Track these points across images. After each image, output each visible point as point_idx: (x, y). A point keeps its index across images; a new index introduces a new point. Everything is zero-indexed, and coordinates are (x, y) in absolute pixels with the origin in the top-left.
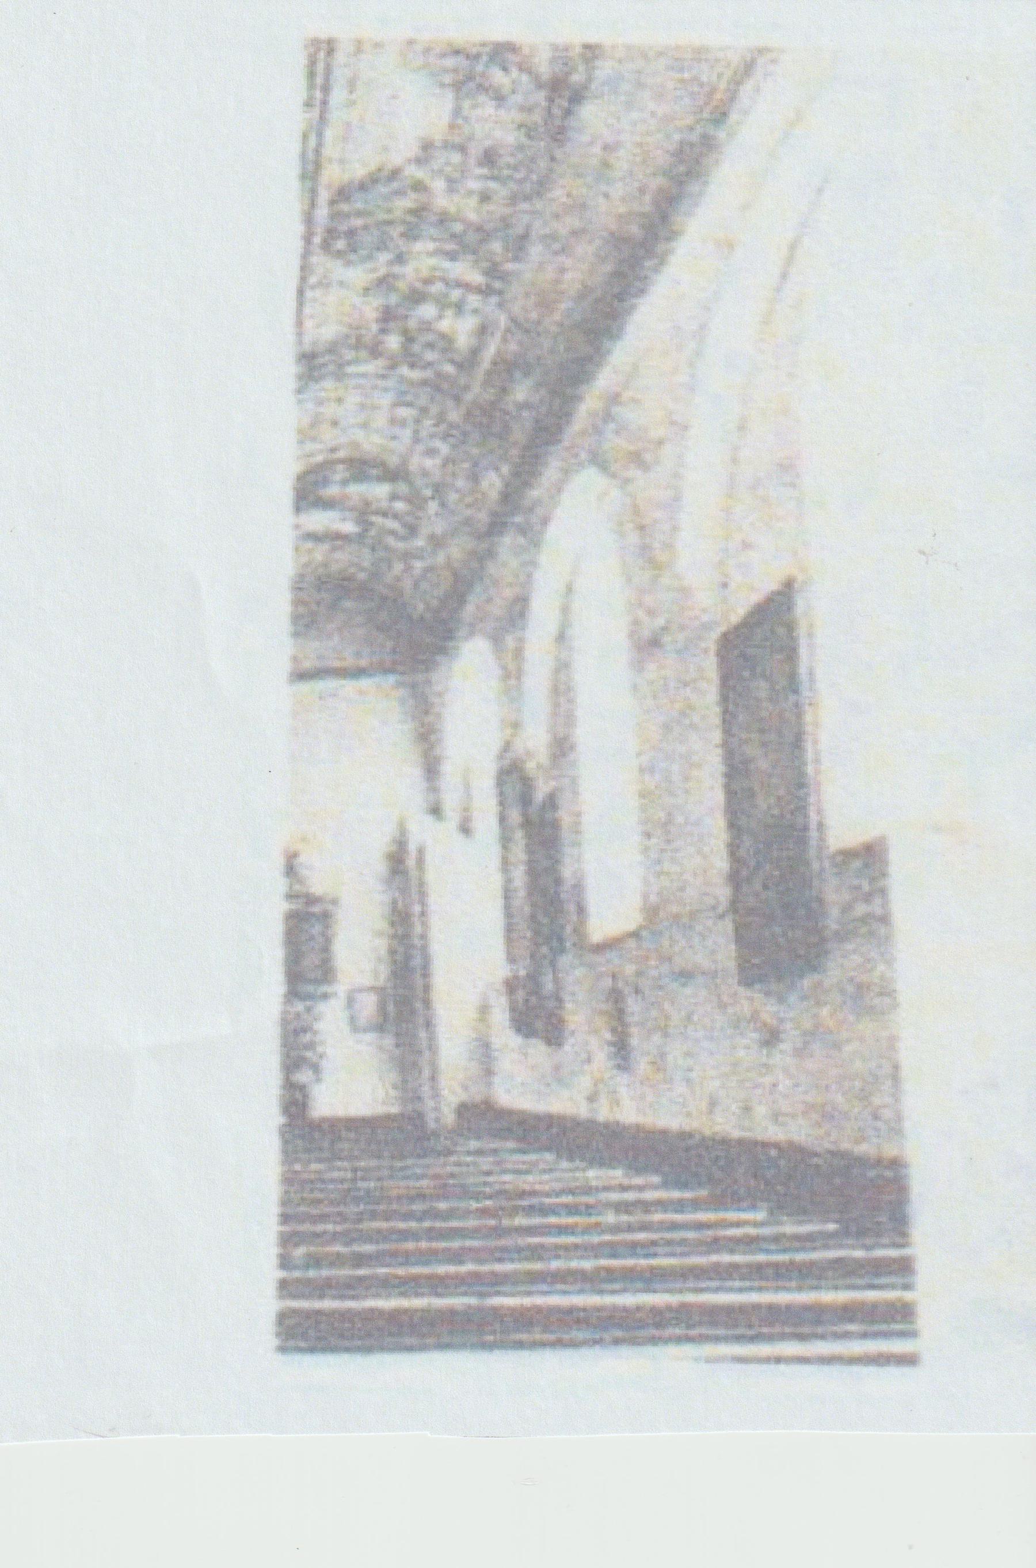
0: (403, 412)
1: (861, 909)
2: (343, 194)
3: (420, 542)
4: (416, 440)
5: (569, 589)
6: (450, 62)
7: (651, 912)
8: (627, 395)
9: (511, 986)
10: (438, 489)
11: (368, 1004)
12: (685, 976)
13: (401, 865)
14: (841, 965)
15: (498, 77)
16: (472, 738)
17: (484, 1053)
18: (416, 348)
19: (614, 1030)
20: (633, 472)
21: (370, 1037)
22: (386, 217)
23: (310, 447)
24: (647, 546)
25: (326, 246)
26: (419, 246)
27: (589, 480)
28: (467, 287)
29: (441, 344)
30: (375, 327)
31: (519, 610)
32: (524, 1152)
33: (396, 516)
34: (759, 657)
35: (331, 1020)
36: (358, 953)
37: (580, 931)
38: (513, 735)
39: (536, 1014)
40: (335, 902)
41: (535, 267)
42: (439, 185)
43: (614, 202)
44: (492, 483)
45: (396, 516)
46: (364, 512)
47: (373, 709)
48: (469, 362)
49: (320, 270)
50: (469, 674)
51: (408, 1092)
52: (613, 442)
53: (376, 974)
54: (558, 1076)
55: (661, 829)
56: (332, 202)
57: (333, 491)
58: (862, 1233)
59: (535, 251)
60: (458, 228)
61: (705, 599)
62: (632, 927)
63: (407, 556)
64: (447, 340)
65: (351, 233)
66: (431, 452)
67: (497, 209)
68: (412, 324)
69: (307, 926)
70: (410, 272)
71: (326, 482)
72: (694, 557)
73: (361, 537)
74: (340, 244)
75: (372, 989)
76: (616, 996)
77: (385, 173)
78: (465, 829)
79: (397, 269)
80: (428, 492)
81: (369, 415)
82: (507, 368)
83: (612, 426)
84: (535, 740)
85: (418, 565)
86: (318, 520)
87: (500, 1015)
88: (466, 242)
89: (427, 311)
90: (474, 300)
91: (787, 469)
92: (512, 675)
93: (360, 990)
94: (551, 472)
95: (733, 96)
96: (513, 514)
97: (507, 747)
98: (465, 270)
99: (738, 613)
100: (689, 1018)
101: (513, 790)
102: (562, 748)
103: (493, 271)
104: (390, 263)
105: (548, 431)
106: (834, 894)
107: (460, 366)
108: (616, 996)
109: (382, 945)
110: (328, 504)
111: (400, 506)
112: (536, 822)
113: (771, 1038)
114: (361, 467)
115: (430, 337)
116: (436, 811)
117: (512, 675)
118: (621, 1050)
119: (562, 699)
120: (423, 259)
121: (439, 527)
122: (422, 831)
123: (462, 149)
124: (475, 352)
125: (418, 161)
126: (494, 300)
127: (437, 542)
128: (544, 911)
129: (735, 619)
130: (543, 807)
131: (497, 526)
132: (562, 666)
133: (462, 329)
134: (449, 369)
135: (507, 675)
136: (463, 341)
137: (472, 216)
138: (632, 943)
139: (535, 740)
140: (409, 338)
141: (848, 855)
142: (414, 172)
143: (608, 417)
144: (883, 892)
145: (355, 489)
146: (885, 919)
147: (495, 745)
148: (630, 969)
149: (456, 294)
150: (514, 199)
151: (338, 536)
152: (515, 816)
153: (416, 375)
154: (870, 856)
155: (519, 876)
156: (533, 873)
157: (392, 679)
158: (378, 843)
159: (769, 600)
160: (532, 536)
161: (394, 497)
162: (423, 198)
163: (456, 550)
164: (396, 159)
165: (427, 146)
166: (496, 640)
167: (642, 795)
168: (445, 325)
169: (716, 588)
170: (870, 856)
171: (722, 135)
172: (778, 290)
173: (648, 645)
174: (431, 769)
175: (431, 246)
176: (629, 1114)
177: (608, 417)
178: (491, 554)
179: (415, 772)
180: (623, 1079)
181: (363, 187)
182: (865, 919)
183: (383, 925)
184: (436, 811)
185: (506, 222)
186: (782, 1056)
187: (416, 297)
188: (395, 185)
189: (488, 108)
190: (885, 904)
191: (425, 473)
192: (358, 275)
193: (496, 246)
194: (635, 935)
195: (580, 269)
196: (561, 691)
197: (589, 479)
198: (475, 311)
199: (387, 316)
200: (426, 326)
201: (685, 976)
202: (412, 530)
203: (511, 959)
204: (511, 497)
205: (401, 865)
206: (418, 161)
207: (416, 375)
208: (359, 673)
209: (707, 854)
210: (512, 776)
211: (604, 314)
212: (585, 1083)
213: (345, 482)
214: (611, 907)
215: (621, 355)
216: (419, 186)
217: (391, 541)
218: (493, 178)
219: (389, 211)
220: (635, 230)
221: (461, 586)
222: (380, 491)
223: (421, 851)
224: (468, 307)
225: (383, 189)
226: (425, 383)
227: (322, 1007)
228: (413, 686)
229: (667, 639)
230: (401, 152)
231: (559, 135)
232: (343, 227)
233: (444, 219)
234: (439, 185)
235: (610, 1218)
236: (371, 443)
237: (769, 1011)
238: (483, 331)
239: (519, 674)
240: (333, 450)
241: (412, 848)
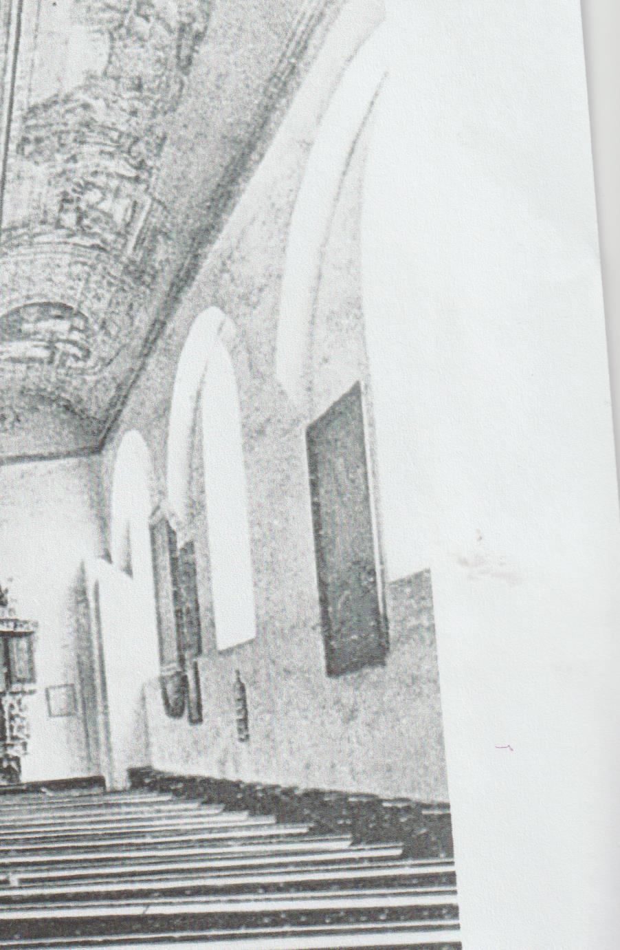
0: (77, 269)
1: (413, 622)
2: (33, 110)
3: (90, 363)
4: (87, 288)
5: (199, 395)
6: (107, 15)
7: (262, 627)
8: (236, 255)
11: (60, 699)
13: (82, 596)
14: (400, 658)
15: (141, 26)
16: (131, 504)
17: (143, 729)
18: (86, 222)
20: (244, 309)
22: (63, 128)
24: (253, 360)
25: (20, 149)
26: (86, 149)
28: (122, 177)
29: (103, 218)
30: (56, 209)
31: (164, 410)
32: (175, 803)
33: (74, 343)
34: (334, 438)
39: (182, 701)
40: (36, 625)
41: (166, 163)
42: (99, 105)
43: (227, 114)
44: (143, 320)
45: (74, 343)
49: (15, 169)
50: (129, 449)
53: (65, 675)
54: (200, 748)
55: (266, 567)
56: (25, 119)
57: (26, 327)
58: (420, 855)
59: (168, 149)
60: (115, 135)
61: (296, 396)
62: (252, 635)
63: (83, 372)
65: (38, 140)
66: (98, 298)
67: (143, 121)
68: (83, 206)
70: (80, 169)
71: (22, 320)
74: (29, 148)
77: (62, 96)
78: (128, 570)
79: (71, 165)
80: (96, 327)
82: (148, 241)
83: (226, 276)
84: (176, 505)
85: (90, 379)
88: (124, 145)
89: (93, 196)
90: (128, 187)
91: (355, 305)
92: (159, 460)
94: (182, 311)
95: (310, 32)
98: (120, 166)
99: (322, 408)
100: (289, 703)
101: (162, 539)
102: (196, 507)
103: (141, 166)
104: (67, 161)
105: (184, 278)
106: (392, 610)
111: (76, 336)
112: (181, 569)
116: (108, 557)
117: (159, 460)
119: (195, 474)
120: (90, 156)
121: (107, 351)
122: (97, 571)
123: (117, 79)
125: (86, 88)
128: (187, 627)
129: (317, 416)
130: (184, 550)
131: (149, 345)
132: (194, 430)
133: (119, 210)
135: (154, 459)
136: (119, 217)
137: (123, 128)
138: (249, 649)
139: (176, 505)
142: (82, 97)
144: (429, 610)
146: (431, 628)
147: (149, 509)
149: (114, 183)
150: (154, 114)
152: (165, 560)
153: (88, 242)
154: (419, 583)
158: (67, 580)
159: (344, 398)
160: (173, 355)
161: (72, 328)
162: (87, 115)
163: (121, 367)
164: (68, 88)
165: (91, 76)
167: (253, 541)
168: (105, 206)
170: (419, 583)
171: (301, 65)
173: (254, 434)
174: (104, 523)
175: (96, 148)
176: (247, 776)
178: (143, 367)
179: (92, 528)
181: (46, 107)
182: (416, 628)
183: (70, 640)
184: (108, 557)
185: (150, 130)
187: (87, 186)
188: (69, 106)
189: (134, 49)
190: (431, 618)
192: (41, 171)
193: (141, 147)
194: (251, 642)
195: (204, 164)
196: (195, 470)
197: (212, 315)
198: (129, 196)
199: (65, 199)
204: (158, 326)
205: (82, 596)
206: (86, 88)
207: (88, 242)
210: (162, 531)
211: (222, 197)
212: (217, 754)
213: (38, 320)
215: (233, 222)
216: (86, 106)
217: (70, 362)
218: (138, 99)
219: (65, 124)
220: (241, 133)
222: (62, 326)
223: (97, 586)
225: (61, 109)
226: (93, 247)
227: (26, 700)
229: (269, 430)
230: (73, 81)
231: (186, 64)
232: (32, 136)
233: (105, 130)
234: (99, 105)
235: (236, 848)
239: (165, 456)
240: (28, 297)
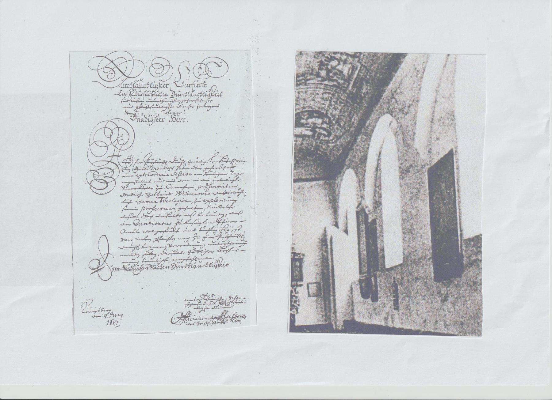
0: (326, 96)
3: (331, 138)
5: (380, 153)
7: (406, 258)
8: (398, 91)
9: (360, 281)
10: (338, 121)
11: (313, 289)
12: (417, 279)
13: (325, 243)
14: (469, 273)
17: (351, 303)
19: (394, 296)
20: (401, 115)
21: (314, 299)
23: (298, 107)
24: (405, 138)
27: (386, 118)
30: (317, 68)
31: (364, 160)
34: (442, 176)
35: (302, 292)
36: (311, 273)
37: (384, 264)
38: (361, 201)
39: (368, 290)
40: (303, 255)
44: (355, 118)
46: (314, 128)
47: (316, 192)
48: (348, 80)
50: (348, 178)
51: (327, 317)
52: (394, 105)
54: (376, 312)
55: (408, 231)
61: (424, 156)
63: (328, 142)
64: (341, 72)
66: (335, 109)
69: (297, 260)
72: (420, 142)
73: (313, 136)
75: (316, 283)
76: (395, 286)
78: (346, 231)
81: (317, 97)
82: (359, 83)
83: (394, 100)
86: (300, 130)
87: (357, 293)
89: (334, 63)
91: (452, 115)
92: (361, 182)
93: (311, 283)
94: (374, 116)
96: (362, 129)
97: (360, 204)
102: (377, 204)
105: (375, 99)
107: (345, 80)
108: (395, 286)
109: (319, 269)
110: (303, 125)
111: (325, 126)
112: (370, 230)
113: (445, 300)
114: (312, 114)
115: (334, 71)
116: (337, 225)
117: (361, 182)
118: (396, 306)
121: (338, 133)
122: (332, 231)
124: (350, 76)
126: (357, 59)
127: (338, 138)
133: (346, 69)
134: (341, 82)
135: (359, 181)
140: (328, 71)
141: (470, 240)
143: (393, 97)
145: (310, 121)
148: (399, 277)
149: (344, 57)
151: (305, 136)
152: (363, 227)
154: (477, 239)
155: (363, 246)
156: (368, 243)
157: (322, 182)
158: (319, 235)
160: (369, 135)
166: (356, 172)
168: (340, 67)
169: (427, 155)
170: (477, 239)
172: (447, 59)
173: (404, 171)
174: (335, 210)
177: (393, 97)
179: (330, 212)
180: (396, 311)
183: (319, 263)
184: (337, 225)
186: (448, 304)
191: (333, 116)
194: (400, 265)
196: (377, 187)
198: (351, 63)
199: (321, 64)
200: (334, 68)
201: (417, 279)
202: (329, 134)
203: (361, 272)
204: (362, 122)
205: (325, 243)
207: (331, 83)
208: (312, 180)
209: (425, 238)
210: (361, 213)
212: (384, 315)
214: (393, 256)
215: (398, 76)
221: (348, 149)
222: (319, 121)
223: (331, 238)
224: (348, 62)
226: (334, 86)
228: (330, 185)
229: (411, 170)
236: (316, 106)
237: (444, 290)
238: (354, 68)
239: (364, 181)
241: (329, 238)
